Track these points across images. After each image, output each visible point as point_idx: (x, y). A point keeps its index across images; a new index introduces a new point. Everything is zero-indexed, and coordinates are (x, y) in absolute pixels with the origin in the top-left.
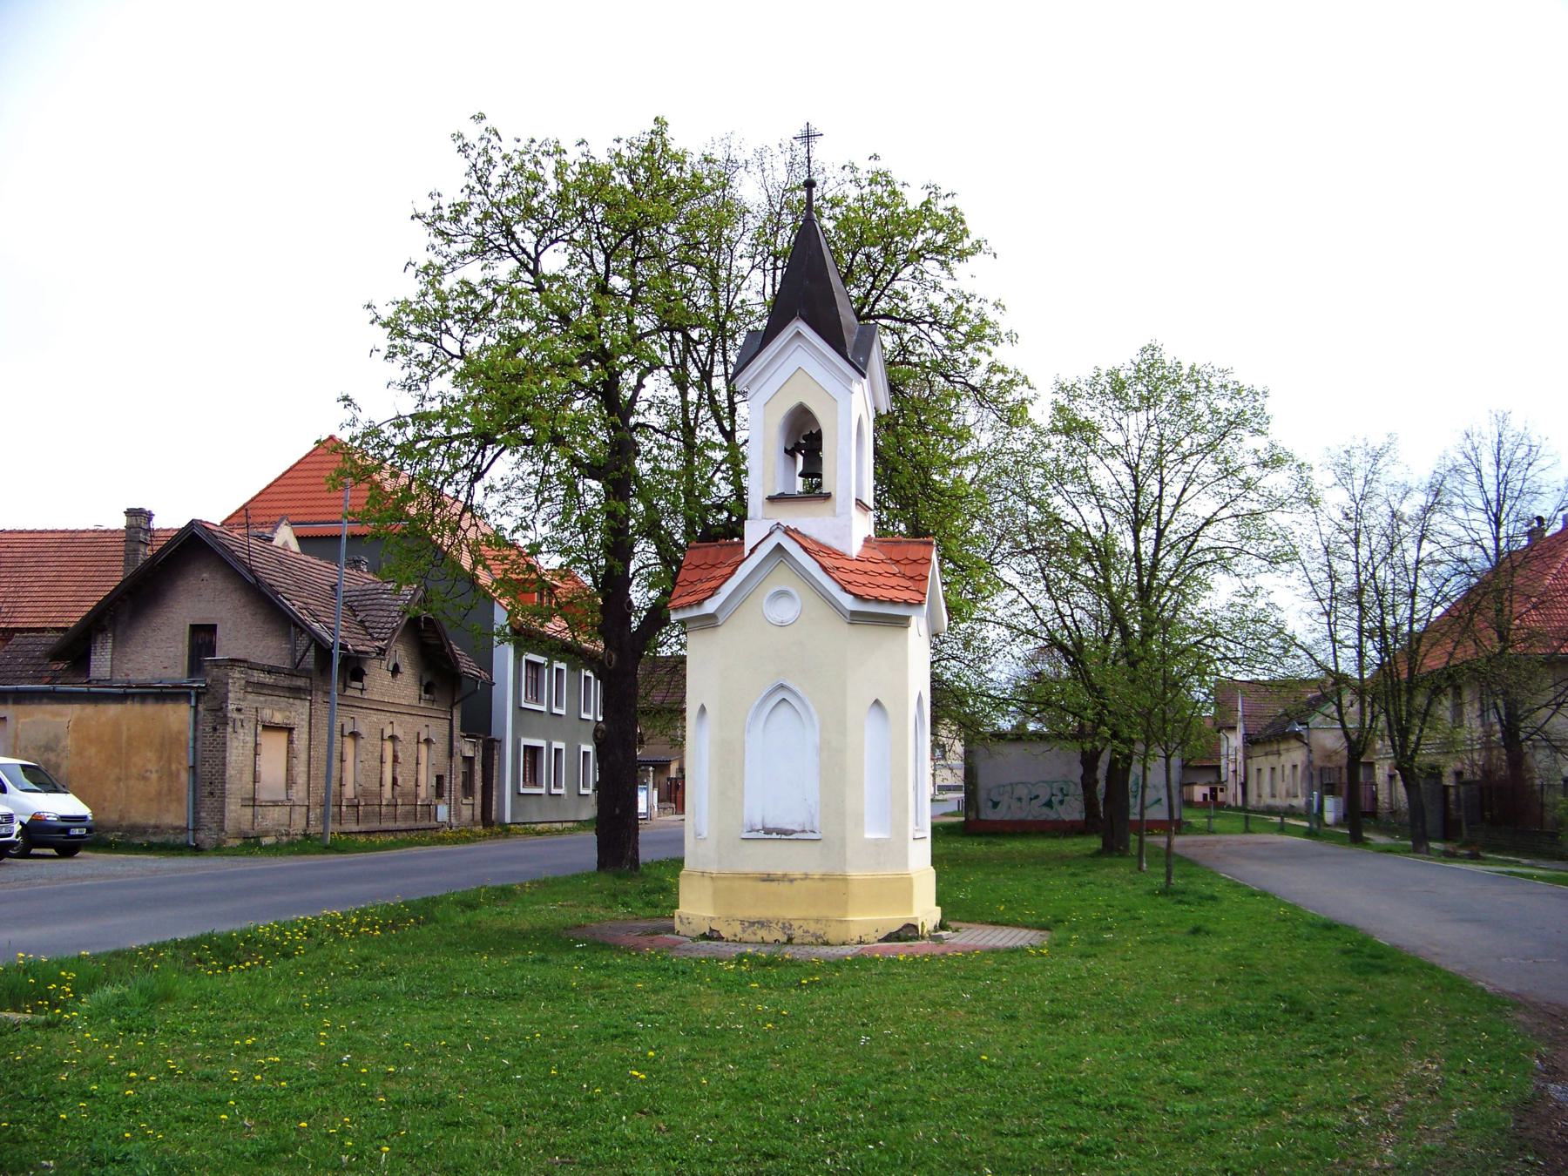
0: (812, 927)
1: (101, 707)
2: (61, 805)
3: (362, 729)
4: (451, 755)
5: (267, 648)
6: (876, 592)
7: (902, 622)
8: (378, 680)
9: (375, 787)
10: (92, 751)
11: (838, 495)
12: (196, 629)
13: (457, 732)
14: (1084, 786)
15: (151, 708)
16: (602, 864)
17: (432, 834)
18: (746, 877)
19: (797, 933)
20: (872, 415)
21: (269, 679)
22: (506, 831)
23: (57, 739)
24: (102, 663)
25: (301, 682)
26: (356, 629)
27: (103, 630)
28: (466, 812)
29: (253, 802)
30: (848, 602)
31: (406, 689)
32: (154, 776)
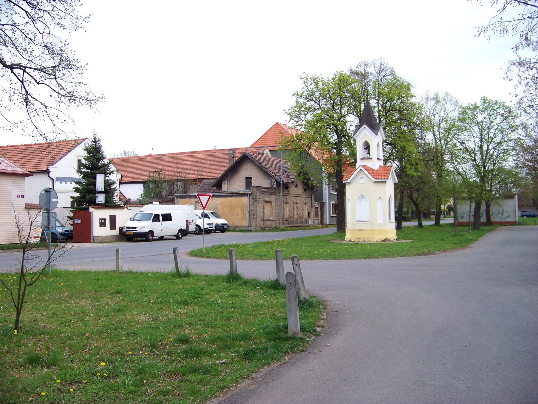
0: (368, 239)
1: (227, 198)
2: (221, 221)
3: (288, 201)
4: (312, 207)
5: (265, 183)
6: (381, 177)
8: (292, 189)
9: (292, 215)
10: (226, 209)
12: (247, 178)
13: (313, 201)
15: (239, 198)
16: (338, 230)
17: (307, 227)
18: (356, 230)
20: (382, 141)
22: (327, 226)
23: (217, 206)
24: (225, 187)
25: (273, 191)
26: (286, 176)
27: (224, 179)
28: (317, 222)
29: (263, 220)
30: (373, 179)
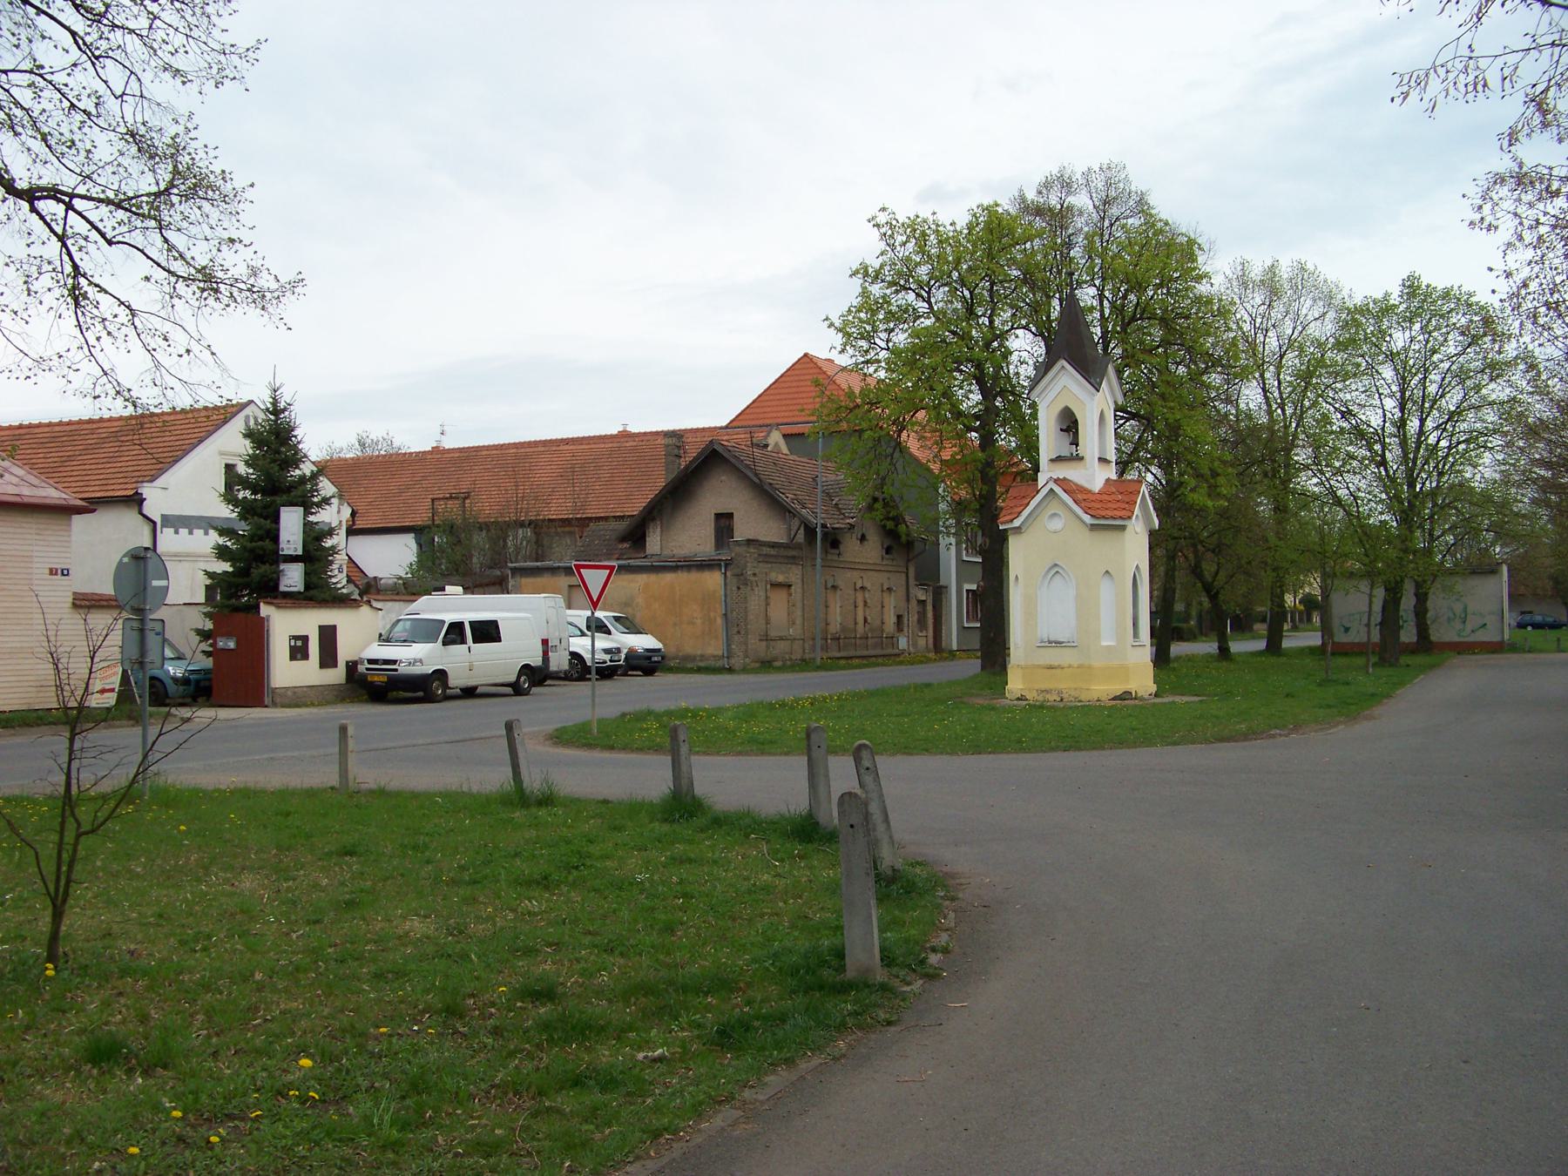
1: (661, 575)
2: (643, 642)
5: (769, 529)
6: (1110, 513)
7: (1123, 528)
8: (851, 547)
9: (851, 626)
11: (1087, 457)
12: (718, 516)
13: (912, 582)
14: (1417, 614)
15: (694, 576)
17: (895, 658)
19: (1065, 696)
21: (772, 552)
25: (794, 553)
27: (653, 519)
28: (922, 642)
29: (766, 638)
30: (1087, 519)
31: (871, 551)
32: (699, 621)
